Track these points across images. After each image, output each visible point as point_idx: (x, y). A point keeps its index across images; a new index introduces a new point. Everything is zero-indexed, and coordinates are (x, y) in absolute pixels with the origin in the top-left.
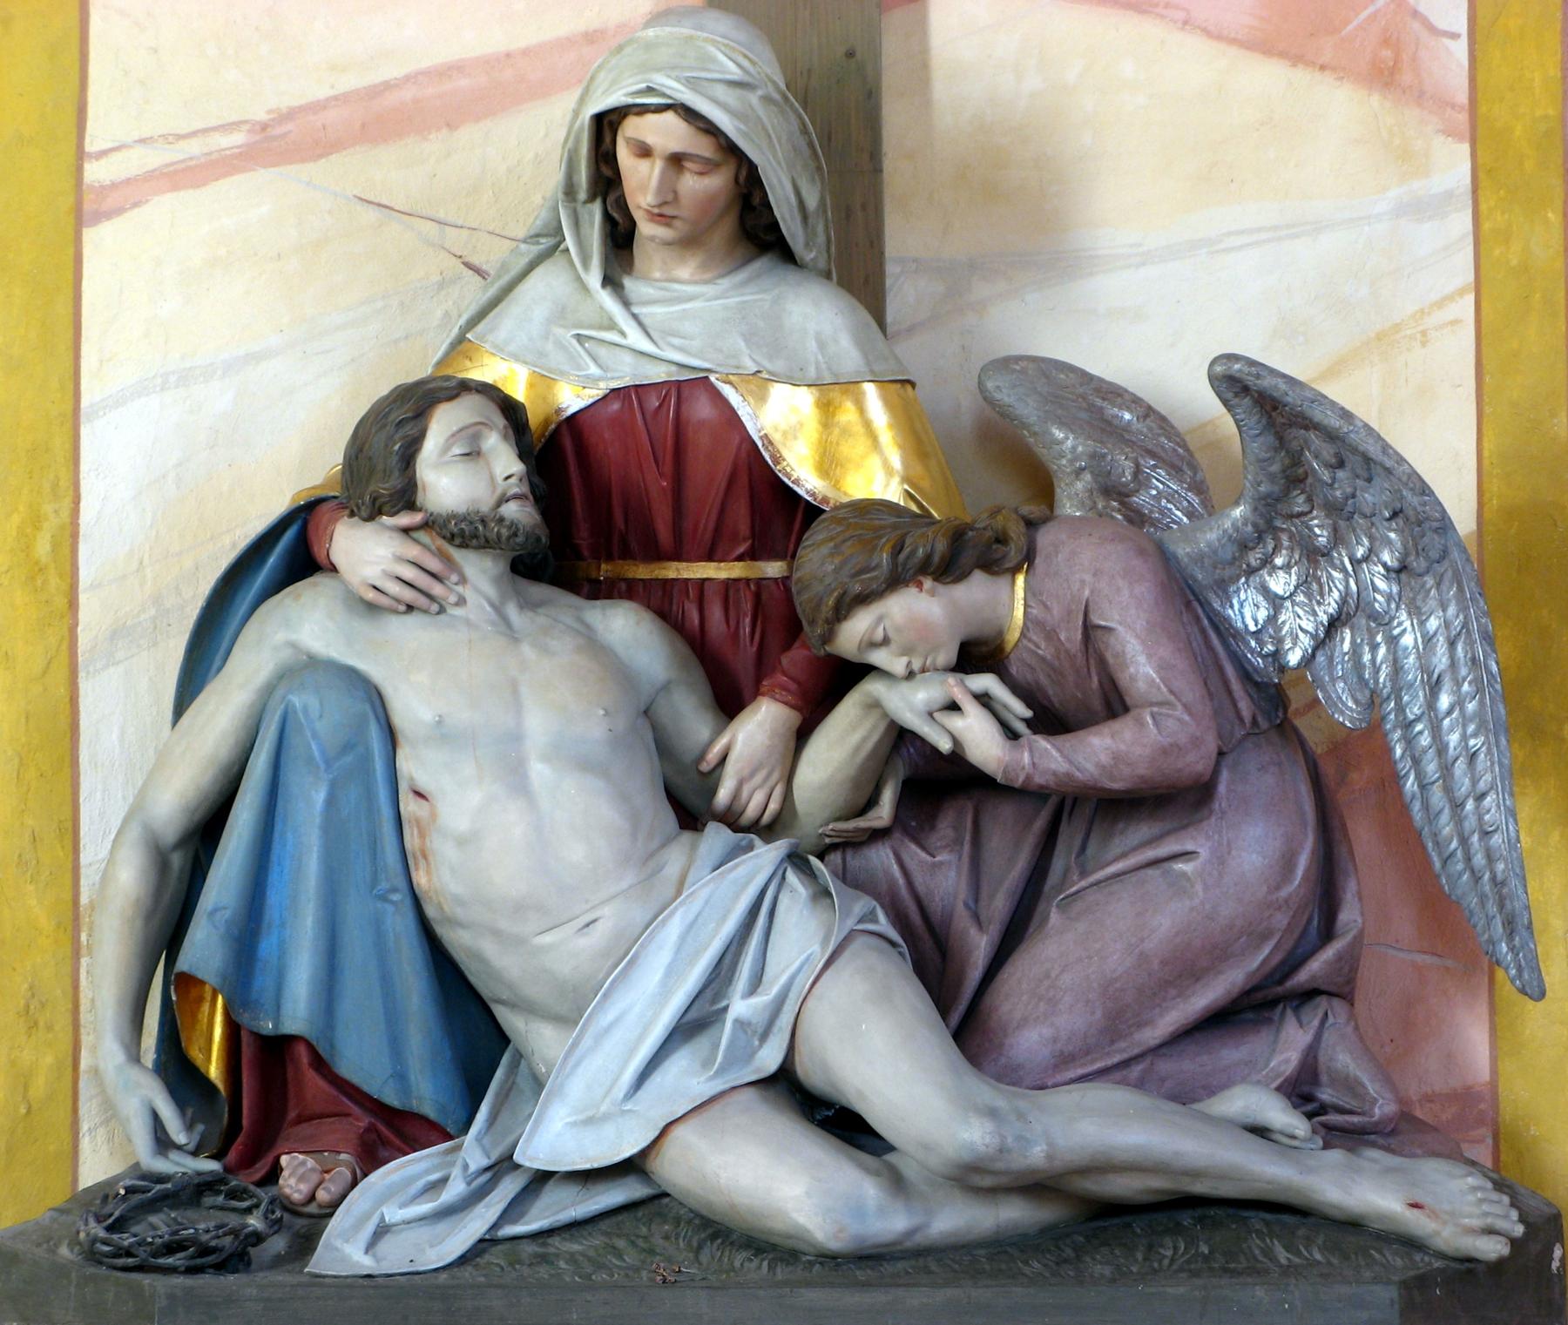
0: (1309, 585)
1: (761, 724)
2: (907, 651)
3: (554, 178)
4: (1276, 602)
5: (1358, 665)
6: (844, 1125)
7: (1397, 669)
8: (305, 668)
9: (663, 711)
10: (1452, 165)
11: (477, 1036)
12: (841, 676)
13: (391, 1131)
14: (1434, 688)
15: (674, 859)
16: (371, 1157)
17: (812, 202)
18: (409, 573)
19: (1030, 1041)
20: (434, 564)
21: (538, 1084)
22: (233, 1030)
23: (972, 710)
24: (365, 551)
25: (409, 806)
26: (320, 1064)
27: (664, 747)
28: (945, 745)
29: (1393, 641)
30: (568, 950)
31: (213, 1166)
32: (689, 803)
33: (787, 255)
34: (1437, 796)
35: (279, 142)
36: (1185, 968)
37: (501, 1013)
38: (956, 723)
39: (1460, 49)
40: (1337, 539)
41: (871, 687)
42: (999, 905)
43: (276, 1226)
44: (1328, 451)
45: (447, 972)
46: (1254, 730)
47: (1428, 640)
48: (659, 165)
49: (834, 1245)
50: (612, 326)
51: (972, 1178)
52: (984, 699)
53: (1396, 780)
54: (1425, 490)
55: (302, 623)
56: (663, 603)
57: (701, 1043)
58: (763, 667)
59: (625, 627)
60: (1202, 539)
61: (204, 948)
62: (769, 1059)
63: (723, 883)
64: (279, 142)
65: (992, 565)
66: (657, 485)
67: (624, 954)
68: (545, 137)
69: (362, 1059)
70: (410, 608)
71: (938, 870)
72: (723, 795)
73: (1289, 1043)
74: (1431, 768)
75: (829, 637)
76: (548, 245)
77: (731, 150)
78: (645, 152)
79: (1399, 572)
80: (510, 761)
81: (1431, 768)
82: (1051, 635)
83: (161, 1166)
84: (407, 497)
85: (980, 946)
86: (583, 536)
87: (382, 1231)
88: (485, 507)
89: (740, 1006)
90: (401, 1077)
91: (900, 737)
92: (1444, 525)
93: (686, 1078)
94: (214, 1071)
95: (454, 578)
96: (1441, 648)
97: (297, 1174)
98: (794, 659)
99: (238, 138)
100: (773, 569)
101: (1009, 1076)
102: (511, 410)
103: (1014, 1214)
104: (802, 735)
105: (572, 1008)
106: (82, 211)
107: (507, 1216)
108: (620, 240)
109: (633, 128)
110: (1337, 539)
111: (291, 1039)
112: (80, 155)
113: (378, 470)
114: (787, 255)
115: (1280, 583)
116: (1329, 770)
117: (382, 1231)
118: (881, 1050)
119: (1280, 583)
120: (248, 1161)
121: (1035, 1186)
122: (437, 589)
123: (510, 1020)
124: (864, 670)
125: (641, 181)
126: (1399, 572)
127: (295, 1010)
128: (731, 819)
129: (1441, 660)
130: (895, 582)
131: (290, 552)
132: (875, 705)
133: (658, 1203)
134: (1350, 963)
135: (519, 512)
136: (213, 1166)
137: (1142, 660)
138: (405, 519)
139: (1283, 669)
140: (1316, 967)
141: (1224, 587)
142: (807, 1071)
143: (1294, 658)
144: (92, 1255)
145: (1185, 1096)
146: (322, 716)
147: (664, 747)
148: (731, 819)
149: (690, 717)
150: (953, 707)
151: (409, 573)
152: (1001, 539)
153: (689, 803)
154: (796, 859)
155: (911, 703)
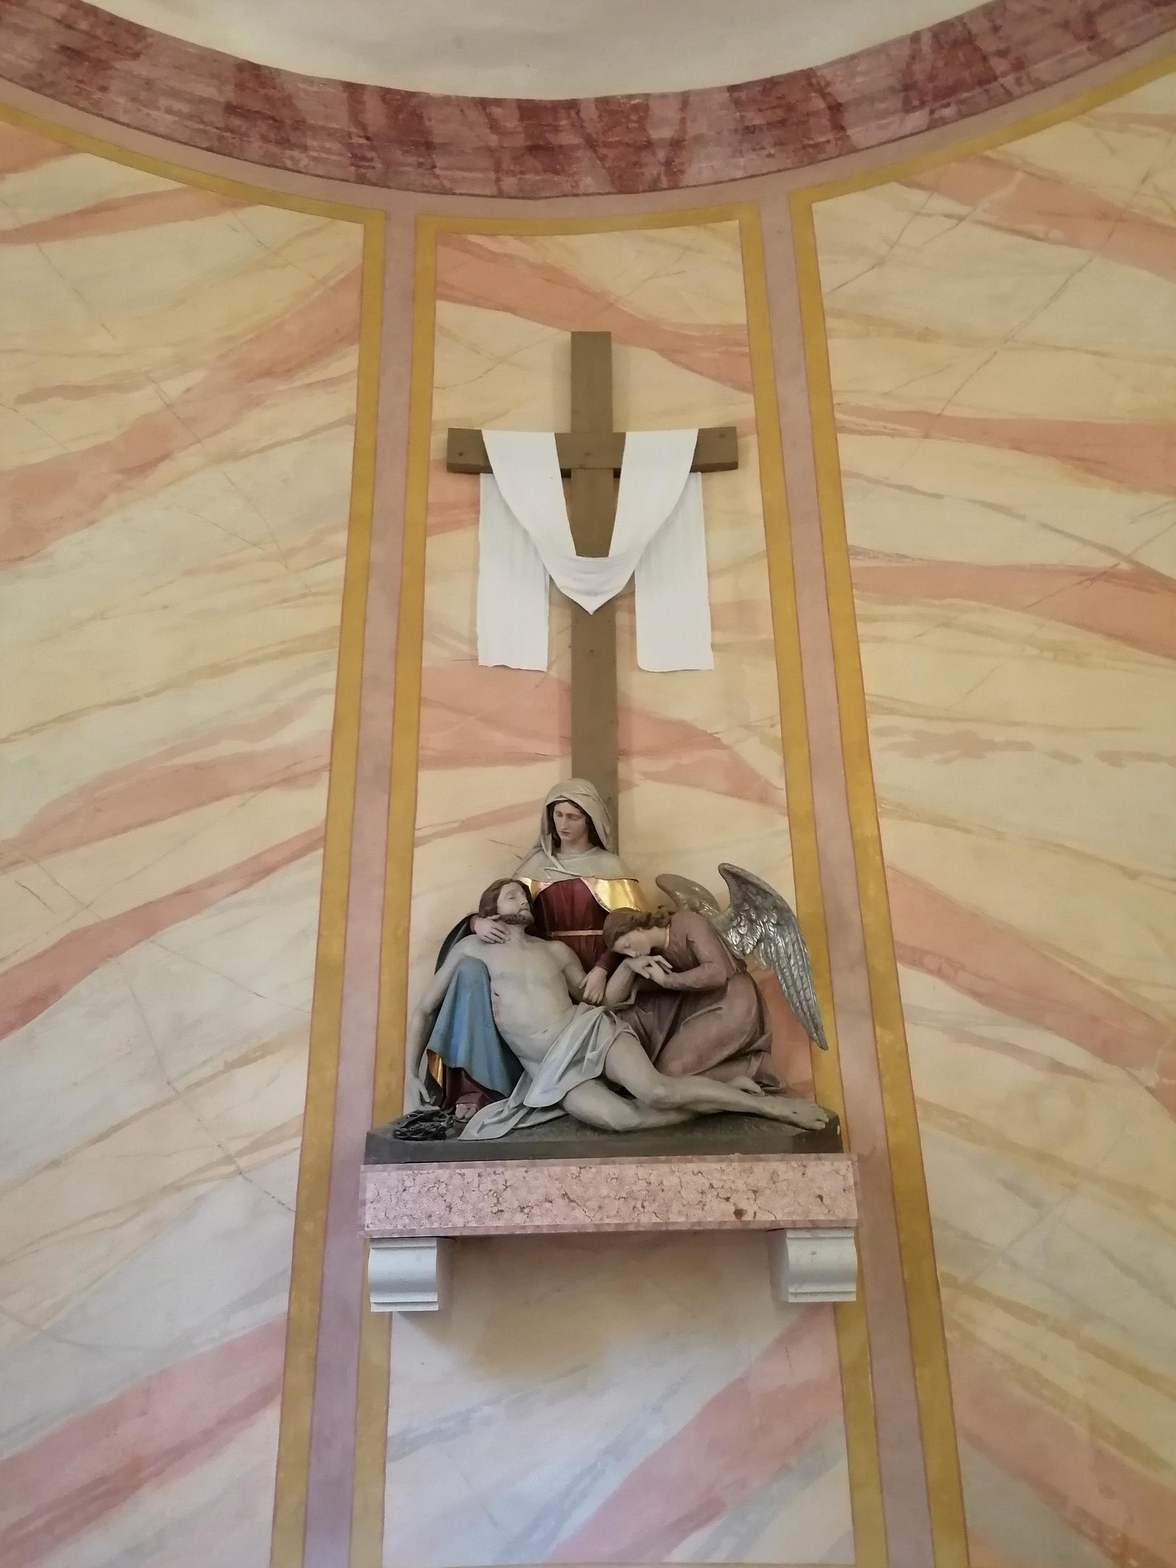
0: (752, 931)
1: (597, 973)
2: (636, 950)
3: (538, 832)
4: (742, 936)
5: (766, 953)
6: (622, 1092)
7: (777, 952)
8: (466, 959)
9: (568, 972)
10: (783, 823)
11: (515, 1068)
12: (619, 958)
13: (490, 1096)
14: (789, 958)
15: (570, 1012)
16: (482, 1103)
17: (608, 831)
18: (495, 931)
19: (675, 1065)
20: (501, 929)
21: (532, 1080)
22: (444, 1066)
23: (656, 966)
24: (483, 927)
25: (494, 997)
26: (469, 1077)
27: (568, 982)
28: (647, 976)
29: (776, 945)
30: (540, 1039)
31: (437, 1108)
32: (576, 998)
33: (603, 847)
34: (792, 990)
35: (466, 826)
36: (721, 1043)
37: (521, 1060)
38: (649, 969)
39: (784, 793)
40: (759, 917)
41: (626, 961)
42: (667, 1026)
43: (451, 1126)
44: (754, 891)
45: (505, 1047)
46: (737, 973)
47: (786, 944)
48: (564, 818)
49: (617, 1128)
50: (554, 865)
51: (659, 1106)
52: (658, 963)
53: (781, 986)
54: (782, 900)
55: (466, 947)
56: (570, 942)
57: (578, 1067)
58: (597, 958)
59: (559, 949)
60: (719, 919)
61: (435, 1043)
62: (598, 1072)
63: (586, 1017)
64: (466, 826)
65: (659, 924)
66: (567, 908)
67: (555, 1040)
68: (535, 824)
69: (481, 1075)
70: (496, 942)
71: (649, 1017)
72: (585, 995)
73: (755, 1064)
74: (790, 982)
75: (613, 946)
76: (539, 848)
77: (584, 812)
78: (561, 815)
79: (777, 925)
80: (526, 986)
81: (790, 982)
82: (677, 944)
83: (422, 1108)
84: (494, 911)
85: (660, 1038)
86: (547, 924)
87: (483, 1126)
88: (516, 912)
89: (589, 1055)
90: (492, 1080)
91: (637, 976)
92: (789, 910)
93: (573, 1078)
94: (439, 1080)
95: (356, 140)
96: (790, 947)
97: (460, 1110)
98: (604, 956)
99: (456, 825)
100: (600, 932)
101: (670, 1074)
102: (525, 887)
103: (673, 1118)
104: (608, 977)
105: (540, 1059)
106: (413, 844)
107: (520, 1121)
108: (557, 844)
109: (557, 808)
110: (759, 917)
111: (460, 1069)
112: (414, 829)
113: (488, 905)
114: (603, 847)
115: (743, 931)
116: (760, 987)
117: (483, 1126)
118: (632, 1066)
119: (743, 931)
120: (447, 1108)
121: (679, 1108)
122: (502, 936)
123: (524, 1062)
124: (625, 956)
125: (560, 823)
126: (777, 925)
127: (460, 1061)
128: (588, 1002)
129: (790, 950)
130: (632, 928)
131: (465, 928)
132: (628, 967)
133: (567, 1116)
134: (770, 1040)
135: (526, 914)
136: (437, 1108)
137: (705, 948)
138: (494, 917)
139: (744, 954)
140: (759, 1043)
141: (726, 931)
142: (609, 1074)
143: (748, 951)
144: (395, 1136)
145: (725, 1080)
146: (469, 973)
147: (568, 982)
148: (588, 1002)
149: (576, 974)
150: (650, 965)
151: (495, 931)
152: (663, 917)
153: (576, 998)
154: (607, 1013)
155: (638, 965)
